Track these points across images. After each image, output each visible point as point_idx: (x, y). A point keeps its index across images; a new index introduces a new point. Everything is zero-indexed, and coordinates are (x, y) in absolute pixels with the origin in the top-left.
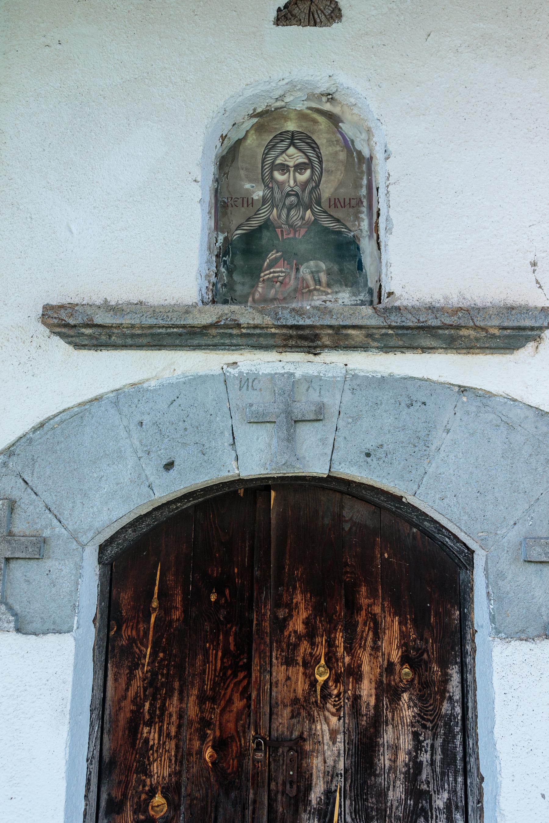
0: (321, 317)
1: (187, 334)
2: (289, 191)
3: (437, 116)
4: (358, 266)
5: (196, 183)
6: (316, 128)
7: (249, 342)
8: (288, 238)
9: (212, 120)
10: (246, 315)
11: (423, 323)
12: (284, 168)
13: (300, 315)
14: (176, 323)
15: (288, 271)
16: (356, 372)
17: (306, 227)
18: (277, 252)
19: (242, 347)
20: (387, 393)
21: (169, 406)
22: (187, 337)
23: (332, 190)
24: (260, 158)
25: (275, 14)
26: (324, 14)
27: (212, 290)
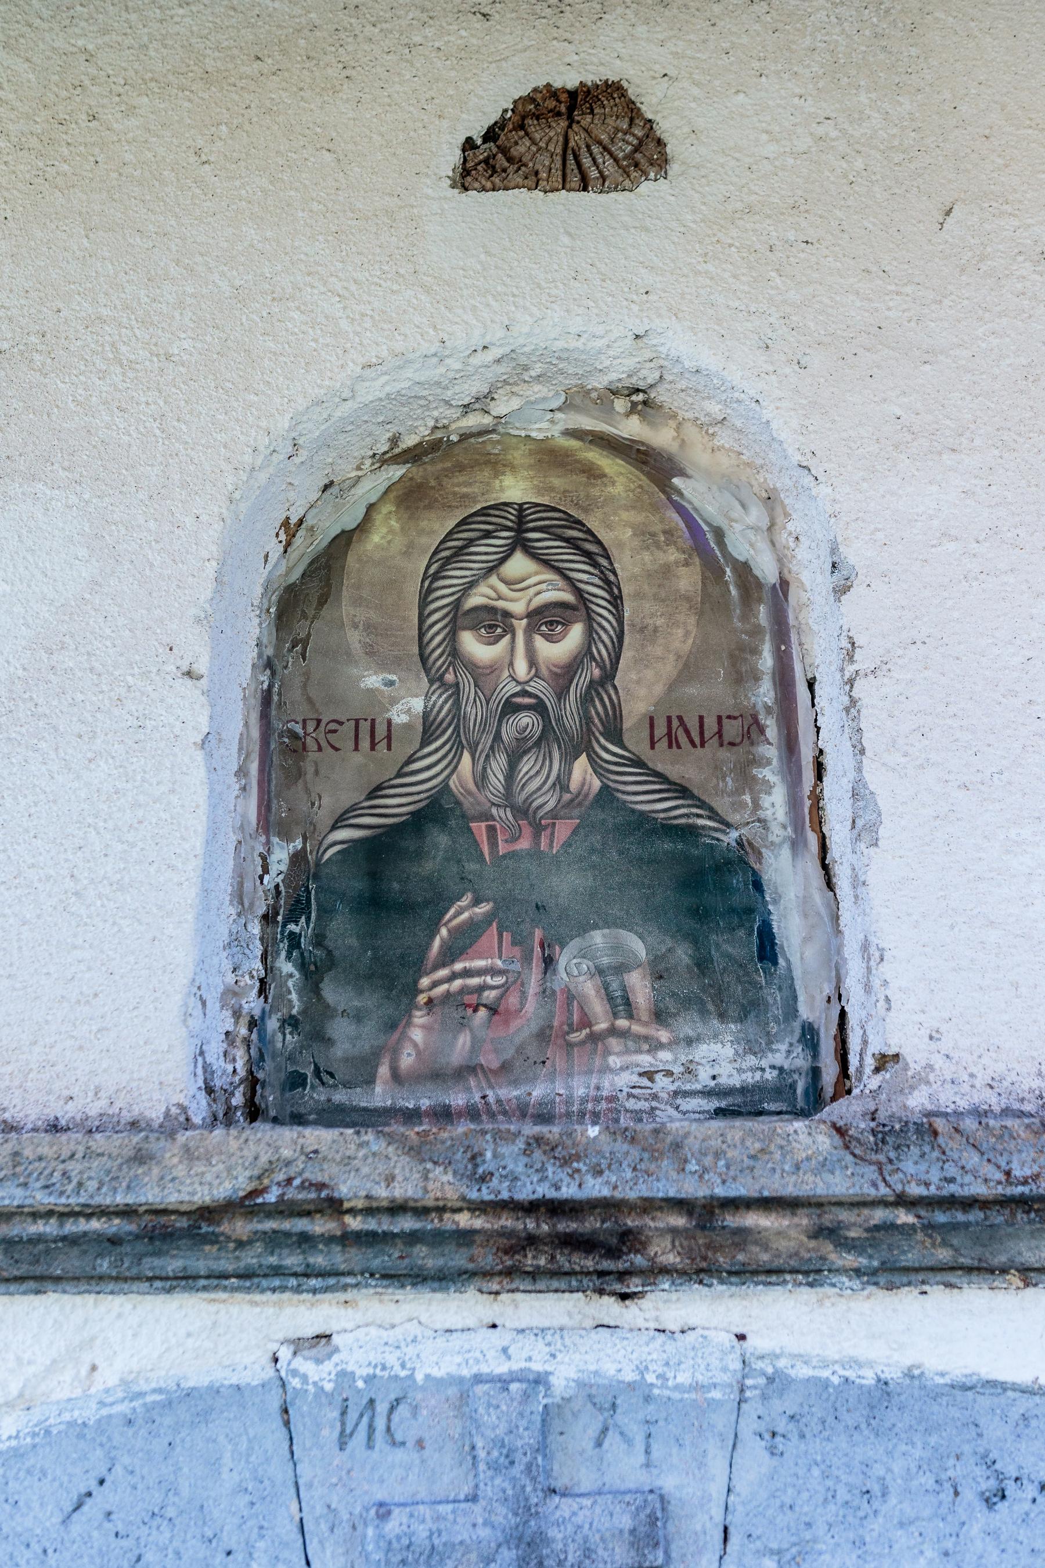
0: (642, 1166)
1: (138, 1237)
2: (514, 695)
3: (996, 452)
4: (761, 947)
5: (189, 682)
6: (595, 492)
7: (376, 1263)
8: (512, 855)
9: (250, 477)
10: (365, 1169)
11: (1025, 1183)
12: (494, 622)
13: (565, 1162)
14: (98, 1200)
15: (517, 966)
16: (782, 1363)
17: (576, 812)
18: (477, 902)
19: (349, 1280)
20: (903, 1448)
21: (66, 1521)
22: (140, 1247)
23: (659, 689)
24: (413, 589)
25: (455, 157)
26: (611, 154)
27: (247, 1042)
